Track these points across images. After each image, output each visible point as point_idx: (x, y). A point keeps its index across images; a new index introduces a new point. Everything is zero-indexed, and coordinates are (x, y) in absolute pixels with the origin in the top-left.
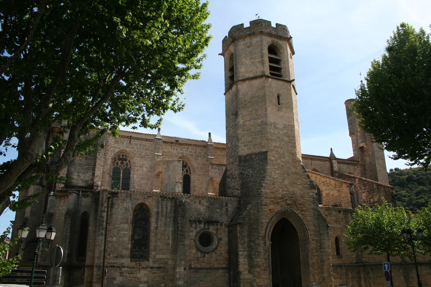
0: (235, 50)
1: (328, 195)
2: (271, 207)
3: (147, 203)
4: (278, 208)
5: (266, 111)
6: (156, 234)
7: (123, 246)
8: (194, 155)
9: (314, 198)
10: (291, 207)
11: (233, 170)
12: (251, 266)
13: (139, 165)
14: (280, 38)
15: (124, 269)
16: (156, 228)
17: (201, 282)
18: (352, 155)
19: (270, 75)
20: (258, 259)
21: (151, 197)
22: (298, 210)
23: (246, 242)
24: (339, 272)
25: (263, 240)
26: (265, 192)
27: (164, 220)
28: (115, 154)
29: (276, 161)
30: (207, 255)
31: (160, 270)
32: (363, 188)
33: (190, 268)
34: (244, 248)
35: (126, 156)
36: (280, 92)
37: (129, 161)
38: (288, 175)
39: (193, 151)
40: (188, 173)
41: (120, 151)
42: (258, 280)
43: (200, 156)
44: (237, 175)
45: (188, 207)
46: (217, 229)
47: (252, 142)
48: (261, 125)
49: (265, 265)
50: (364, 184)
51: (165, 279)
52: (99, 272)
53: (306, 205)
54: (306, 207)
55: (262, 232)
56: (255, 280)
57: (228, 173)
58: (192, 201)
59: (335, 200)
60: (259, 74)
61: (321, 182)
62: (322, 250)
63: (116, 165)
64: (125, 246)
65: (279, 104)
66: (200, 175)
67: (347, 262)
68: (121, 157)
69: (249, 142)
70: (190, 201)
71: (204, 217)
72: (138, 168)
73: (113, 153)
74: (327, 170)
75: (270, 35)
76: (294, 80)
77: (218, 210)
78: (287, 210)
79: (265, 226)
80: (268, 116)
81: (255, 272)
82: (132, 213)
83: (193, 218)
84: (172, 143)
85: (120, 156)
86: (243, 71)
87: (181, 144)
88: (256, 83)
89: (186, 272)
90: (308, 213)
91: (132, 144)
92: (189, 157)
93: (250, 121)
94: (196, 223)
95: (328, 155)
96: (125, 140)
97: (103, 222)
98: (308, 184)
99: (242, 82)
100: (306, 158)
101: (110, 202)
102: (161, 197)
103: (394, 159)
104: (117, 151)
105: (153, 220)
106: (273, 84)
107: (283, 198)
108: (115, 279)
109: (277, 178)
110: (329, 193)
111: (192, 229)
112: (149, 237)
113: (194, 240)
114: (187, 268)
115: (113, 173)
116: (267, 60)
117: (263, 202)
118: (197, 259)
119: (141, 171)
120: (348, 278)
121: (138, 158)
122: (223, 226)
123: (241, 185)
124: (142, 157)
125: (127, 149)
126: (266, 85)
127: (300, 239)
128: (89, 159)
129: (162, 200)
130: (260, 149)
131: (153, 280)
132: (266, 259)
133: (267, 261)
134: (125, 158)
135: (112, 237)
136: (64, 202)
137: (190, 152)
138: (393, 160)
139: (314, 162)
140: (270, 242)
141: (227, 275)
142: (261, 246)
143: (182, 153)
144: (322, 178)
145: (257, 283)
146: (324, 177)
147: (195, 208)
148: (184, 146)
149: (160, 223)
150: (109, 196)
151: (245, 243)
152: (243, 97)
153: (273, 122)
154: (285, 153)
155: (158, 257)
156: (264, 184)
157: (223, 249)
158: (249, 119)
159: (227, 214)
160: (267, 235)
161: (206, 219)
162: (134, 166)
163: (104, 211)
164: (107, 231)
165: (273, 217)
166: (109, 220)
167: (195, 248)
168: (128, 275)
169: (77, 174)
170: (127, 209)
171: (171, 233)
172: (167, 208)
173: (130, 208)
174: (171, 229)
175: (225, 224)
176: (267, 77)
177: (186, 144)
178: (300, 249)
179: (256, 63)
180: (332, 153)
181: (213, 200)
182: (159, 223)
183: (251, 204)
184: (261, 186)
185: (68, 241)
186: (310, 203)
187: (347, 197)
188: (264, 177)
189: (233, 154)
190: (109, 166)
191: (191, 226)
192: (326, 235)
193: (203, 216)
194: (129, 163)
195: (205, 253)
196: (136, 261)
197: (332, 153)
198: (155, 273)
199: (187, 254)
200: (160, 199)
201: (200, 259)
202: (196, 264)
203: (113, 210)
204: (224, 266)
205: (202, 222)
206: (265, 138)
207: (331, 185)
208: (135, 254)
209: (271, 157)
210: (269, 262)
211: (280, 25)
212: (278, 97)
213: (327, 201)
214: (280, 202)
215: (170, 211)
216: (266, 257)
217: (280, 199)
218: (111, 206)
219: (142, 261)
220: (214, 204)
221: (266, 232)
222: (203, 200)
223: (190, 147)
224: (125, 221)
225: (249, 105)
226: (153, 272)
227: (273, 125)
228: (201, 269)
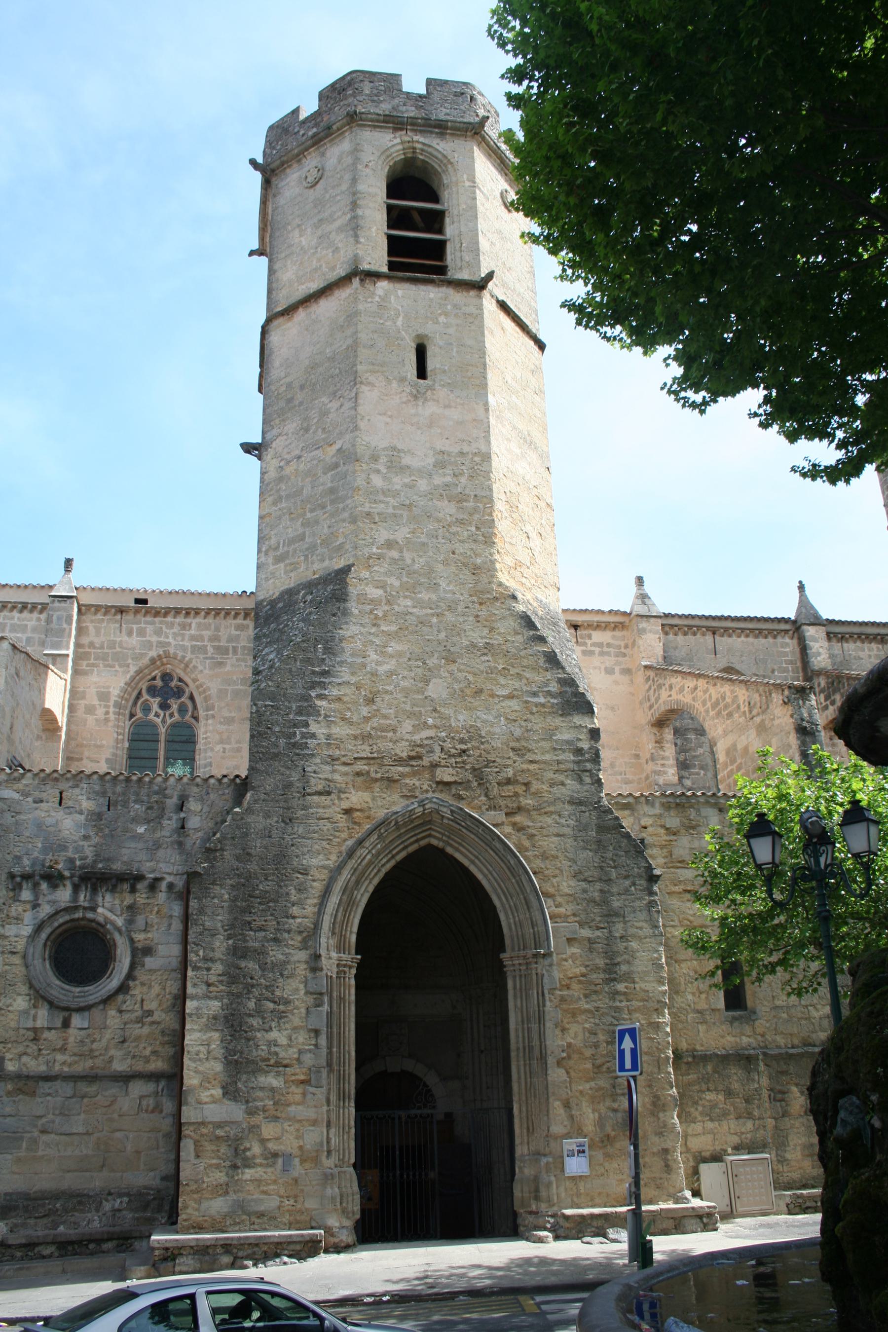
2: (357, 798)
4: (389, 804)
5: (355, 408)
8: (210, 650)
10: (460, 798)
12: (239, 1066)
14: (441, 128)
17: (45, 1138)
20: (274, 1035)
23: (218, 955)
24: (736, 1086)
25: (304, 946)
26: (329, 737)
29: (388, 602)
30: (77, 1021)
34: (209, 985)
36: (429, 329)
38: (450, 659)
39: (207, 633)
40: (188, 717)
42: (269, 1130)
46: (131, 908)
47: (302, 537)
48: (336, 466)
49: (308, 1059)
53: (535, 786)
54: (537, 794)
55: (303, 913)
56: (254, 1129)
58: (26, 795)
61: (709, 704)
62: (621, 987)
66: (229, 721)
67: (781, 1040)
69: (292, 541)
70: (16, 796)
71: (72, 861)
74: (785, 670)
75: (395, 123)
76: (490, 276)
77: (141, 830)
78: (438, 811)
79: (318, 886)
80: (362, 425)
81: (260, 1094)
83: (26, 862)
84: (121, 610)
87: (157, 613)
88: (326, 307)
90: (549, 820)
92: (189, 656)
93: (299, 457)
94: (36, 885)
95: (790, 612)
98: (549, 693)
99: (286, 317)
100: (690, 627)
103: (804, 475)
106: (407, 303)
107: (419, 757)
109: (390, 674)
110: (734, 745)
111: (15, 909)
113: (24, 957)
118: (31, 1034)
120: (785, 1114)
122: (162, 897)
126: (361, 307)
127: (508, 941)
132: (317, 1032)
133: (323, 1041)
137: (193, 638)
138: (821, 485)
139: (724, 642)
140: (351, 958)
142: (291, 976)
143: (160, 644)
145: (263, 1141)
147: (40, 826)
148: (169, 619)
151: (212, 960)
152: (283, 374)
153: (383, 444)
154: (440, 567)
156: (322, 703)
158: (297, 452)
159: (180, 844)
165: (360, 842)
167: (24, 989)
175: (171, 886)
176: (373, 276)
177: (177, 611)
179: (333, 236)
180: (804, 602)
181: (119, 789)
183: (253, 788)
186: (561, 778)
187: (789, 746)
188: (325, 673)
191: (16, 899)
192: (643, 915)
193: (70, 854)
195: (67, 1009)
197: (804, 602)
201: (46, 1034)
202: (25, 1059)
205: (61, 877)
206: (346, 515)
209: (363, 587)
210: (330, 1047)
211: (444, 83)
214: (402, 775)
216: (319, 1020)
217: (400, 761)
220: (125, 804)
222: (77, 791)
223: (194, 622)
227: (383, 460)
228: (47, 1078)
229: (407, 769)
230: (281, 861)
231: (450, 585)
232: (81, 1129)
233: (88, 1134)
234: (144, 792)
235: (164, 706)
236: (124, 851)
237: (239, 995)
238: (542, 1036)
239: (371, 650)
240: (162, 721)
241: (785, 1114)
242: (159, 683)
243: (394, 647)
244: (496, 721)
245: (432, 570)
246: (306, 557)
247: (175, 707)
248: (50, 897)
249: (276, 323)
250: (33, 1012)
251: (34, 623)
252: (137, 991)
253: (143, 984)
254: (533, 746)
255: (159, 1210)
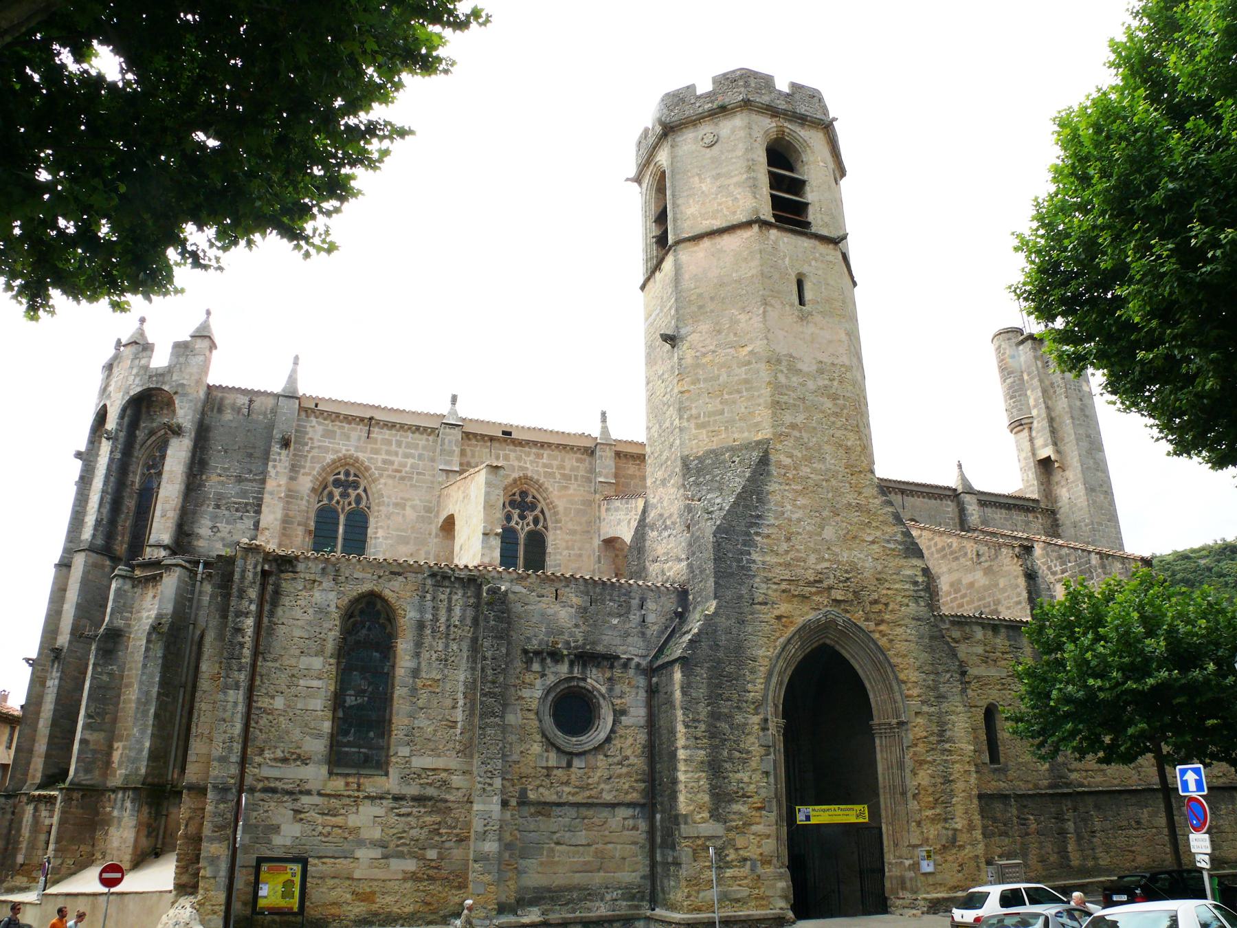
0: (673, 158)
1: (955, 586)
2: (784, 608)
3: (387, 593)
4: (805, 615)
6: (414, 691)
7: (306, 725)
8: (558, 476)
9: (916, 583)
11: (665, 504)
12: (721, 798)
13: (394, 500)
14: (803, 120)
15: (305, 800)
16: (415, 673)
17: (558, 847)
18: (1021, 486)
19: (773, 220)
20: (739, 775)
21: (400, 574)
22: (867, 620)
23: (702, 717)
24: (998, 815)
26: (764, 563)
27: (441, 647)
28: (324, 469)
29: (795, 469)
30: (577, 763)
31: (424, 806)
32: (1058, 569)
33: (523, 802)
34: (696, 739)
35: (356, 475)
36: (805, 269)
37: (365, 490)
40: (539, 527)
41: (340, 459)
43: (576, 479)
44: (675, 516)
45: (518, 608)
46: (610, 679)
47: (722, 412)
48: (749, 363)
50: (1060, 557)
51: (440, 835)
52: (222, 806)
57: (652, 515)
59: (980, 600)
60: (742, 217)
61: (933, 549)
62: (947, 746)
63: (325, 501)
64: (312, 725)
65: (802, 302)
66: (573, 532)
68: (342, 477)
70: (524, 591)
72: (391, 509)
73: (318, 467)
75: (771, 111)
82: (337, 623)
83: (535, 642)
84: (492, 439)
85: (339, 473)
86: (691, 214)
89: (508, 814)
91: (376, 440)
96: (354, 429)
97: (242, 645)
101: (270, 588)
102: (433, 575)
104: (328, 460)
105: (404, 646)
107: (820, 581)
108: (276, 829)
109: (799, 520)
110: (959, 581)
111: (529, 677)
112: (392, 699)
114: (513, 802)
115: (317, 522)
116: (764, 180)
117: (756, 595)
119: (400, 519)
121: (390, 482)
122: (631, 672)
123: (690, 545)
124: (402, 478)
125: (361, 456)
127: (875, 713)
128: (247, 480)
129: (437, 585)
130: (746, 434)
131: (401, 838)
132: (767, 773)
133: (772, 780)
134: (354, 482)
135: (273, 697)
136: (154, 597)
137: (545, 466)
139: (910, 501)
141: (643, 825)
144: (937, 539)
146: (941, 534)
147: (543, 615)
149: (427, 655)
150: (266, 567)
155: (418, 763)
156: (759, 538)
157: (631, 744)
158: (712, 348)
159: (643, 634)
160: (770, 698)
161: (576, 648)
162: (379, 505)
163: (247, 615)
164: (258, 678)
166: (262, 641)
167: (538, 737)
168: (320, 819)
169: (210, 524)
170: (322, 611)
171: (461, 688)
172: (449, 610)
173: (333, 609)
174: (462, 678)
176: (764, 224)
177: (535, 443)
178: (877, 741)
182: (425, 655)
184: (750, 543)
185: (152, 711)
187: (1017, 586)
189: (666, 454)
190: (304, 502)
191: (528, 669)
194: (363, 495)
195: (571, 754)
196: (348, 775)
198: (409, 815)
199: (515, 757)
200: (429, 582)
201: (555, 772)
202: (541, 790)
203: (279, 611)
204: (634, 796)
205: (563, 656)
207: (966, 554)
208: (347, 753)
211: (801, 87)
212: (800, 284)
213: (955, 604)
214: (810, 593)
215: (462, 620)
217: (810, 584)
218: (271, 599)
219: (367, 776)
221: (767, 689)
222: (568, 589)
223: (546, 453)
224: (315, 647)
225: (710, 306)
226: (403, 811)
227: (784, 363)
229: (814, 590)
230: (738, 651)
231: (833, 461)
232: (584, 842)
233: (589, 845)
234: (616, 593)
235: (522, 517)
236: (604, 637)
237: (717, 747)
238: (903, 778)
239: (786, 503)
240: (523, 529)
241: (1027, 834)
242: (517, 497)
243: (801, 501)
244: (867, 557)
245: (820, 448)
246: (726, 428)
247: (531, 518)
248: (553, 669)
249: (682, 246)
250: (546, 754)
251: (424, 442)
252: (617, 743)
253: (621, 736)
254: (889, 578)
255: (642, 899)
